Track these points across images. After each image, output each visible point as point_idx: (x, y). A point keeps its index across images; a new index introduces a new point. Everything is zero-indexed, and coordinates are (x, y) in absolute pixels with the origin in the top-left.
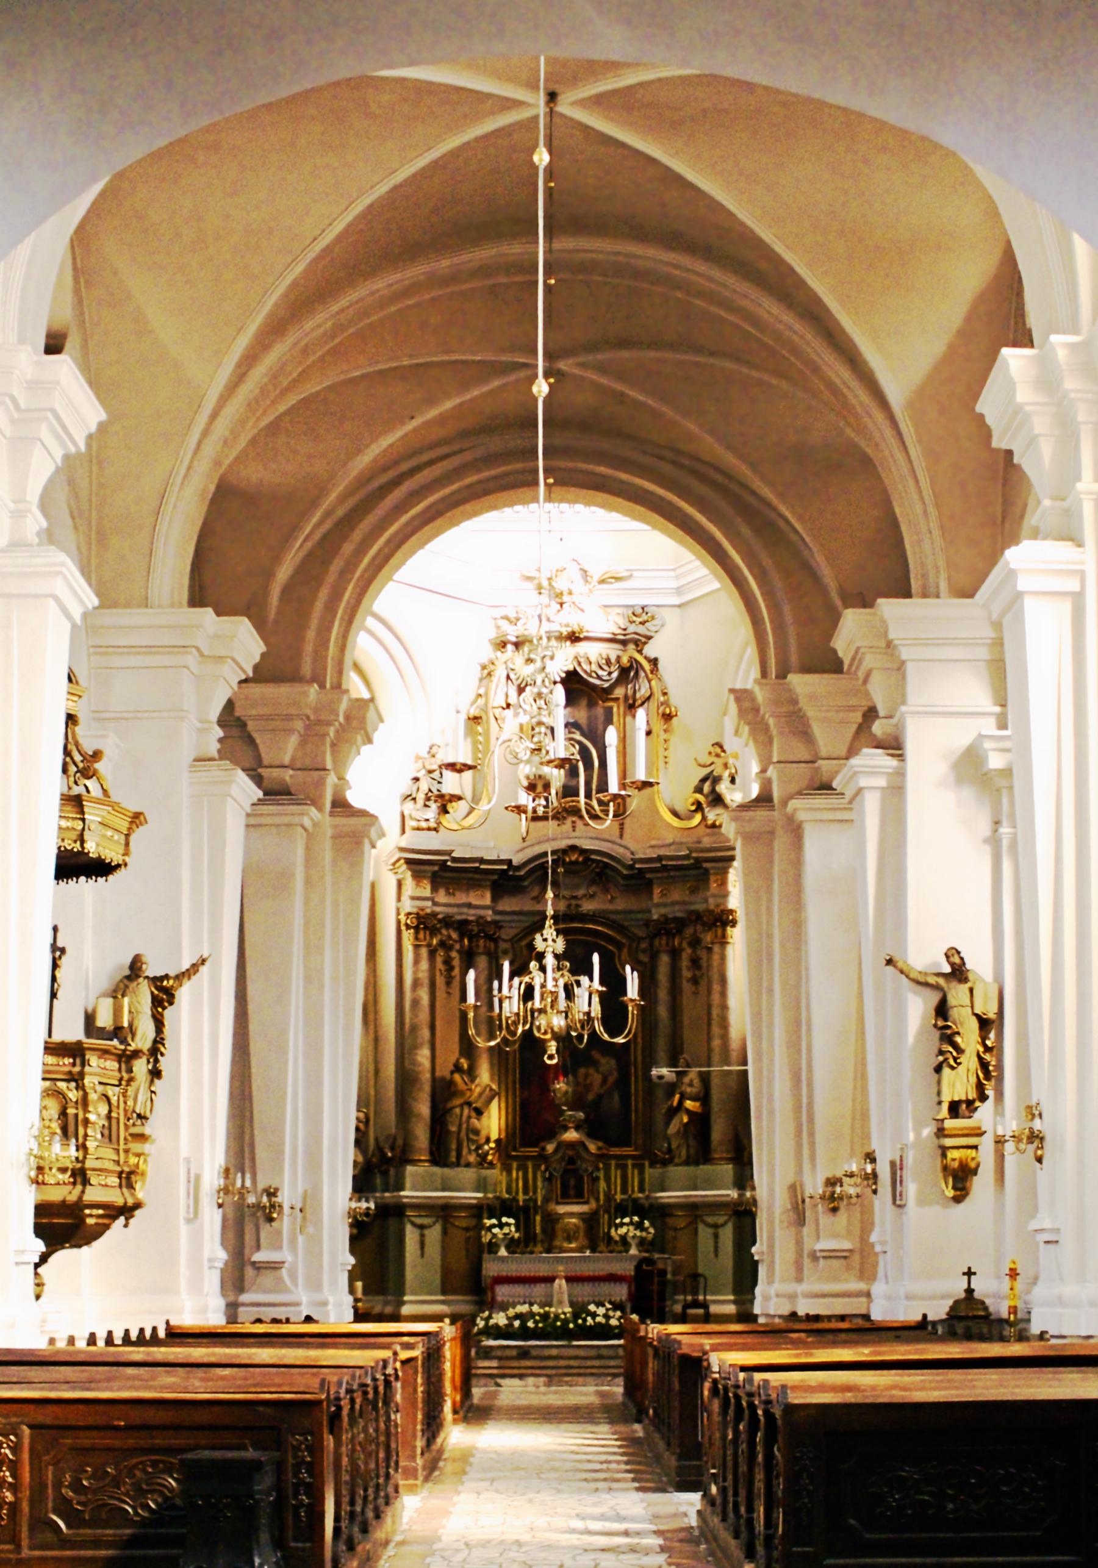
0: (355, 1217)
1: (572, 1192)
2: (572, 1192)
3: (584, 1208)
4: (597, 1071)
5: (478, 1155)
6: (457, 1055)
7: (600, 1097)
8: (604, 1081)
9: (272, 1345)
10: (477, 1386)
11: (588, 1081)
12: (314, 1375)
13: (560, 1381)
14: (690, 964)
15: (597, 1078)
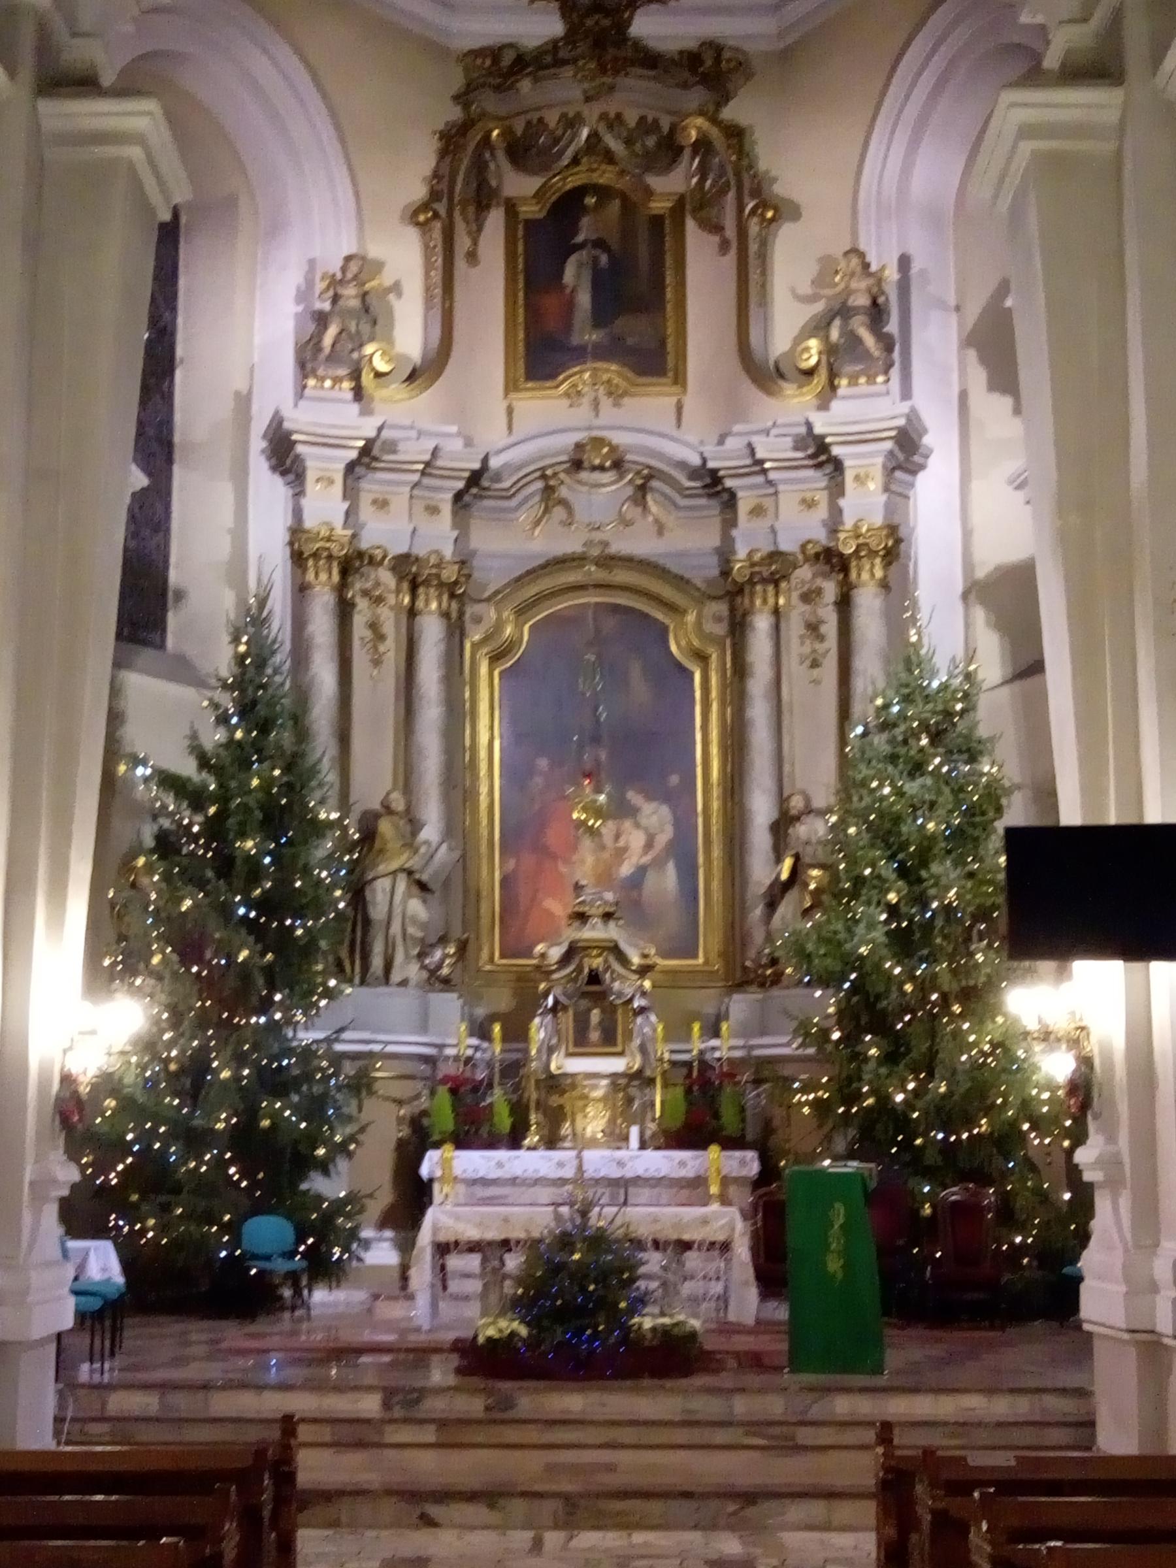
0: (111, 975)
1: (595, 1035)
2: (595, 1035)
3: (617, 1065)
4: (637, 825)
5: (423, 967)
6: (388, 785)
7: (642, 871)
8: (649, 845)
9: (379, 1343)
10: (308, 1525)
11: (621, 843)
12: (135, 1368)
13: (403, 1332)
14: (803, 631)
15: (635, 840)
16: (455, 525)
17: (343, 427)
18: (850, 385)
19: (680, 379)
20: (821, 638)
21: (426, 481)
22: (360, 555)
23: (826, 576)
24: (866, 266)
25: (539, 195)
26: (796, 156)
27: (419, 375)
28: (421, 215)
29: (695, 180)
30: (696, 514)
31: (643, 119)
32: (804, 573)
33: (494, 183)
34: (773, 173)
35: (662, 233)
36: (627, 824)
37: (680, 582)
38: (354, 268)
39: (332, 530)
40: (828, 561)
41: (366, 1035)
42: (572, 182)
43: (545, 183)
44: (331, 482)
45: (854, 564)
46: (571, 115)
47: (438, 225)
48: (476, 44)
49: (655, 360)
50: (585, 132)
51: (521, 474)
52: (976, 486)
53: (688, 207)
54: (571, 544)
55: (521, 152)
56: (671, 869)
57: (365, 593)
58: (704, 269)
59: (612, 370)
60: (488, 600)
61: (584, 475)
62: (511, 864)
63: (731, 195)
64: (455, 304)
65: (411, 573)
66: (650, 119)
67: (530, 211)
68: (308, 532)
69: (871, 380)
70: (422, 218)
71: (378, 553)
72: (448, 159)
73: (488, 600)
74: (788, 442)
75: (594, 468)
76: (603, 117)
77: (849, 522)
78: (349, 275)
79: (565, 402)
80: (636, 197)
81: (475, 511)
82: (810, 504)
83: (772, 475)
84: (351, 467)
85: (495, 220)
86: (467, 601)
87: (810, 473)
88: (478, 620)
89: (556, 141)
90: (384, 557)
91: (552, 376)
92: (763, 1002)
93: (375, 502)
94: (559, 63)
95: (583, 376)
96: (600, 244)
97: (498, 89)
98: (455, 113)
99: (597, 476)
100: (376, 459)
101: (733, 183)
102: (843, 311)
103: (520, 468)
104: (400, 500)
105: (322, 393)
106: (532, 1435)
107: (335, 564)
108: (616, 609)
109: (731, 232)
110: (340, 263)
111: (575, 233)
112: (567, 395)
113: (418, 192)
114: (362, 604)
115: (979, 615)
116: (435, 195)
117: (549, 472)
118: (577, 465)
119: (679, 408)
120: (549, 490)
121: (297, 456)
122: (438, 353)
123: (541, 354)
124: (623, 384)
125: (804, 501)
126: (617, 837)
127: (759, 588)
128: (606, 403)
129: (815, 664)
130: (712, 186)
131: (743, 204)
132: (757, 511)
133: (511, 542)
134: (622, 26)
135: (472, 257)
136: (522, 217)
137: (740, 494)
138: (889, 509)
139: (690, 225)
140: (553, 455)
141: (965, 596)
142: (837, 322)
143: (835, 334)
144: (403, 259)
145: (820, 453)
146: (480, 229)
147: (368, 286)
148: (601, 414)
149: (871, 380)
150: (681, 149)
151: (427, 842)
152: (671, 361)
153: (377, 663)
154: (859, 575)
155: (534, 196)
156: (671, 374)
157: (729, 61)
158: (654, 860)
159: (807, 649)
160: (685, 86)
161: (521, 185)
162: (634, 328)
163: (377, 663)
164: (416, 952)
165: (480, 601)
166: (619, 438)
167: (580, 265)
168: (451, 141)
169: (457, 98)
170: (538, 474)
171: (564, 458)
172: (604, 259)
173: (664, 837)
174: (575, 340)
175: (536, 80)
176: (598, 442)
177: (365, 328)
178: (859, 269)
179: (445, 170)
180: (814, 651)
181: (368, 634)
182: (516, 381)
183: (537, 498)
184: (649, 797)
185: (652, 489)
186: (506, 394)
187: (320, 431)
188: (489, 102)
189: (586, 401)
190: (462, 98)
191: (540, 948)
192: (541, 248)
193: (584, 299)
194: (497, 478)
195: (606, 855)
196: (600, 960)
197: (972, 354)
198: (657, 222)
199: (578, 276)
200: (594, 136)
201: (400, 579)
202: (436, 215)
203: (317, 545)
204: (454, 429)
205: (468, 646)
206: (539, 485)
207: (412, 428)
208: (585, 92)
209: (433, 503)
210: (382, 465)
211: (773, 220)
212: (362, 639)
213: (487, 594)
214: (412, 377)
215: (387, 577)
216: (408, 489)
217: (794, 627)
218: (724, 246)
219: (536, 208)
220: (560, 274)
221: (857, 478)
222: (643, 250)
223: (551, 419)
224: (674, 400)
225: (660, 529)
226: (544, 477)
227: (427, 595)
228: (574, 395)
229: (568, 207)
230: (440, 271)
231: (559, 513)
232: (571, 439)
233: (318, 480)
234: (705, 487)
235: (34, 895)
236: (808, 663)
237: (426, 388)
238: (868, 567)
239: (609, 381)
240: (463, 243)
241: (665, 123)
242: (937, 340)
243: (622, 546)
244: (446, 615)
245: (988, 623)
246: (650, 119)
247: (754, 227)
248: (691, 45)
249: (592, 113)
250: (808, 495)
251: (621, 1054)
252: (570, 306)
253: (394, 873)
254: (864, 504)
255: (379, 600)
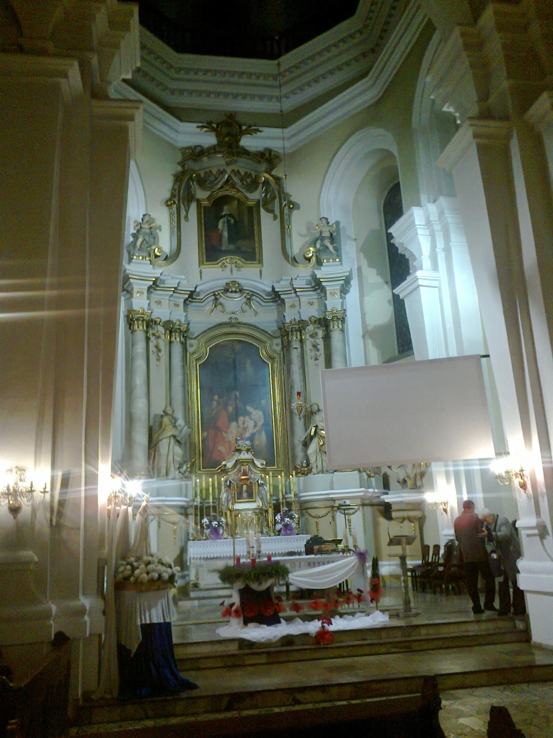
1: (245, 495)
2: (245, 495)
3: (253, 506)
4: (251, 419)
8: (255, 426)
11: (245, 425)
14: (311, 348)
15: (251, 424)
16: (184, 311)
17: (148, 273)
18: (333, 261)
19: (261, 262)
20: (318, 350)
21: (175, 295)
22: (152, 320)
23: (318, 328)
24: (328, 223)
25: (209, 199)
26: (296, 188)
27: (169, 259)
28: (168, 203)
29: (263, 195)
30: (269, 308)
31: (246, 173)
32: (311, 328)
33: (193, 193)
34: (290, 194)
35: (252, 213)
36: (247, 418)
37: (264, 332)
38: (146, 218)
39: (144, 310)
40: (319, 323)
41: (163, 498)
42: (221, 194)
43: (211, 195)
44: (143, 293)
45: (331, 323)
46: (222, 170)
47: (175, 206)
48: (185, 145)
49: (252, 255)
50: (227, 176)
51: (207, 293)
52: (366, 299)
53: (261, 205)
54: (225, 319)
55: (202, 183)
56: (264, 434)
57: (154, 335)
58: (268, 225)
59: (236, 259)
60: (195, 338)
61: (229, 294)
62: (205, 434)
63: (277, 201)
64: (182, 233)
65: (170, 328)
66: (249, 173)
67: (205, 203)
68: (135, 311)
69: (334, 260)
70: (169, 203)
71: (158, 320)
72: (178, 183)
73: (195, 338)
74: (304, 282)
75: (232, 292)
76: (233, 171)
77: (329, 309)
78: (145, 221)
79: (221, 269)
80: (243, 199)
81: (189, 307)
82: (311, 304)
83: (298, 293)
84: (149, 288)
85: (193, 206)
86: (187, 339)
87: (312, 293)
88: (191, 346)
89: (216, 179)
90: (160, 322)
91: (216, 260)
92: (304, 479)
93: (156, 302)
94: (216, 152)
95: (227, 260)
96: (230, 215)
97: (195, 161)
98: (179, 168)
99: (233, 295)
100: (157, 286)
101: (277, 195)
102: (322, 238)
103: (206, 292)
104: (165, 303)
105: (139, 261)
106: (337, 652)
107: (145, 322)
108: (240, 341)
109: (277, 212)
110: (141, 216)
111: (222, 211)
112: (221, 266)
113: (168, 195)
114: (153, 338)
115: (370, 342)
116: (173, 196)
117: (216, 293)
118: (226, 290)
119: (261, 272)
120: (216, 299)
121: (130, 283)
122: (177, 250)
123: (211, 252)
124: (241, 263)
125: (309, 303)
126: (244, 423)
127: (336, 323)
128: (235, 270)
129: (316, 359)
130: (270, 197)
131: (281, 203)
132: (293, 306)
133: (202, 318)
134: (238, 141)
135: (186, 218)
136: (203, 205)
137: (286, 300)
138: (342, 303)
139: (262, 210)
140: (219, 287)
141: (363, 337)
142: (319, 241)
143: (318, 246)
144: (163, 218)
145: (317, 285)
146: (189, 208)
147: (151, 226)
148: (233, 273)
149: (334, 260)
150: (259, 183)
151: (180, 425)
152: (257, 256)
153: (158, 360)
154: (333, 327)
155: (207, 198)
156: (258, 260)
157: (274, 155)
158: (257, 431)
159: (313, 354)
160: (259, 162)
161: (202, 194)
162: (244, 244)
163: (158, 360)
164: (177, 466)
165: (192, 339)
166: (240, 281)
167: (224, 223)
168: (178, 178)
169: (179, 163)
170: (213, 294)
171: (223, 288)
172: (232, 221)
173: (261, 423)
174: (223, 248)
175: (209, 158)
176: (234, 282)
177: (152, 240)
178: (326, 224)
179: (176, 187)
180: (316, 354)
181: (155, 350)
182: (203, 262)
183: (212, 302)
184: (255, 409)
185: (252, 299)
186: (199, 266)
187: (144, 275)
188: (190, 164)
189: (228, 269)
190: (182, 164)
191: (224, 463)
192: (209, 217)
193: (226, 234)
194: (198, 295)
195: (240, 430)
196: (247, 467)
197: (362, 255)
198: (250, 209)
199: (224, 226)
200: (229, 177)
201: (166, 329)
202: (174, 202)
203: (139, 316)
204: (184, 277)
205: (188, 354)
206: (213, 297)
207: (169, 276)
208: (226, 162)
209: (177, 303)
210: (158, 288)
211: (292, 208)
212: (153, 351)
213: (194, 337)
214: (166, 258)
215: (161, 329)
216: (168, 297)
217: (308, 346)
218: (275, 218)
219: (208, 203)
220: (217, 226)
221: (331, 294)
222: (246, 219)
223: (216, 275)
224: (258, 269)
225: (256, 313)
226: (215, 295)
227: (175, 335)
228: (224, 266)
229: (219, 202)
230: (176, 223)
231: (219, 307)
232: (224, 282)
233: (138, 293)
234: (272, 299)
235: (98, 435)
236: (314, 358)
237: (172, 263)
238: (336, 324)
239: (236, 263)
240: (183, 213)
241: (253, 175)
242: (350, 249)
243: (243, 319)
244: (181, 343)
245: (373, 345)
246: (249, 173)
247: (286, 211)
248: (261, 149)
249: (229, 170)
250: (311, 301)
251: (255, 501)
252: (221, 236)
253: (170, 437)
254: (333, 303)
255: (158, 337)
